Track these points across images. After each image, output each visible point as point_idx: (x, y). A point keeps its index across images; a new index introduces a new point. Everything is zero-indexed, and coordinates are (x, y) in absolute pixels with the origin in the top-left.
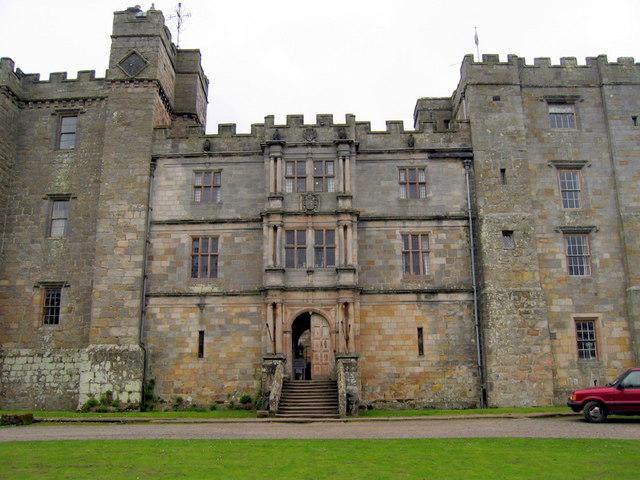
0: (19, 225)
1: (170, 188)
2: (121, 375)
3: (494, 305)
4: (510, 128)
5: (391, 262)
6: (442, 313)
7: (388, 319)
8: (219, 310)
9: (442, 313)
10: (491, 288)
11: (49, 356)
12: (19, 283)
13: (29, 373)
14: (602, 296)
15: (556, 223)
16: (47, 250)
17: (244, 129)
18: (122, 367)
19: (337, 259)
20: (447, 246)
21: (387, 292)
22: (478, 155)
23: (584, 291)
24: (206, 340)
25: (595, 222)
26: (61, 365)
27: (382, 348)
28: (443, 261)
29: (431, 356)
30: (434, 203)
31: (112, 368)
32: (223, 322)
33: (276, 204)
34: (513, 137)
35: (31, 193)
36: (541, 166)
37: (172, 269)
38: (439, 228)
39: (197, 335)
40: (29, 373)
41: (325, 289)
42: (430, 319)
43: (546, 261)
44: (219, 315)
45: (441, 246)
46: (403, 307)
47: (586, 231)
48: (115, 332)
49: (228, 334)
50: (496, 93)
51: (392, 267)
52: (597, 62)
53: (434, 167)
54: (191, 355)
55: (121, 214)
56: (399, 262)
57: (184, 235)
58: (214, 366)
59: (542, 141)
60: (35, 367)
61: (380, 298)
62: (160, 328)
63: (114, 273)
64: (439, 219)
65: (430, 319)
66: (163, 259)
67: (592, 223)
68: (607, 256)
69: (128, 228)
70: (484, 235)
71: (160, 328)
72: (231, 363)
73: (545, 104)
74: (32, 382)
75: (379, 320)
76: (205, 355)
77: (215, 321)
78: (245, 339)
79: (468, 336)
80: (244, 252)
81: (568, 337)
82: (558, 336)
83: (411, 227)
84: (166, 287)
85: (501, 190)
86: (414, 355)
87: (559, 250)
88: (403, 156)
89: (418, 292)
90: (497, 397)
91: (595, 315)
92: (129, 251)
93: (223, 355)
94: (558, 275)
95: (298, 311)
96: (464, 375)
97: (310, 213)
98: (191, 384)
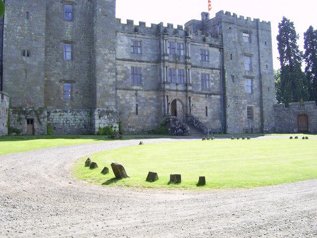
0: (50, 52)
1: (122, 45)
2: (111, 120)
3: (229, 100)
4: (234, 40)
6: (213, 102)
7: (197, 103)
9: (213, 102)
10: (227, 94)
11: (70, 112)
12: (52, 79)
13: (62, 119)
14: (254, 99)
15: (244, 74)
16: (64, 66)
17: (148, 25)
18: (111, 118)
20: (214, 79)
22: (225, 48)
24: (139, 108)
25: (254, 75)
26: (76, 116)
29: (210, 117)
30: (211, 63)
31: (108, 118)
32: (144, 101)
35: (54, 38)
37: (125, 79)
39: (135, 106)
40: (62, 119)
42: (209, 104)
46: (202, 99)
48: (107, 104)
49: (146, 106)
52: (257, 21)
53: (211, 49)
54: (133, 113)
55: (106, 55)
56: (200, 83)
57: (129, 66)
58: (142, 117)
59: (241, 45)
60: (64, 117)
62: (122, 102)
63: (106, 79)
64: (212, 69)
65: (209, 104)
66: (121, 75)
67: (253, 76)
69: (109, 61)
70: (226, 76)
71: (122, 102)
72: (148, 117)
74: (64, 124)
76: (139, 113)
77: (142, 101)
78: (152, 108)
79: (220, 110)
80: (151, 74)
81: (245, 112)
84: (123, 86)
85: (231, 61)
86: (204, 116)
89: (206, 94)
90: (229, 130)
91: (252, 105)
92: (110, 70)
93: (145, 114)
98: (134, 124)
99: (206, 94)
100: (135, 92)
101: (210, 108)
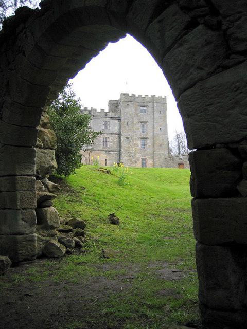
25: (148, 136)
50: (128, 104)
59: (138, 116)
64: (112, 134)
85: (127, 128)
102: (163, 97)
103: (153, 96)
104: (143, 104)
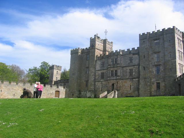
1: (98, 65)
5: (127, 74)
7: (126, 84)
8: (104, 83)
12: (83, 81)
14: (161, 78)
15: (154, 64)
19: (183, 55)
20: (135, 70)
21: (126, 79)
23: (158, 77)
25: (161, 63)
27: (125, 89)
28: (134, 73)
29: (132, 90)
33: (109, 66)
34: (146, 49)
36: (151, 54)
38: (134, 68)
39: (101, 87)
41: (115, 79)
42: (132, 84)
43: (151, 72)
44: (104, 84)
45: (134, 71)
46: (128, 82)
47: (160, 65)
50: (144, 41)
51: (127, 75)
53: (134, 56)
61: (125, 80)
64: (134, 66)
66: (97, 76)
67: (160, 64)
68: (162, 70)
69: (92, 72)
73: (153, 41)
75: (125, 84)
82: (153, 86)
83: (130, 68)
86: (129, 90)
87: (154, 70)
88: (129, 55)
89: (130, 79)
92: (93, 75)
94: (153, 74)
95: (112, 83)
96: (136, 92)
97: (114, 67)
99: (130, 79)
100: (101, 82)
101: (133, 85)
102: (172, 27)
103: (163, 30)
104: (155, 38)
